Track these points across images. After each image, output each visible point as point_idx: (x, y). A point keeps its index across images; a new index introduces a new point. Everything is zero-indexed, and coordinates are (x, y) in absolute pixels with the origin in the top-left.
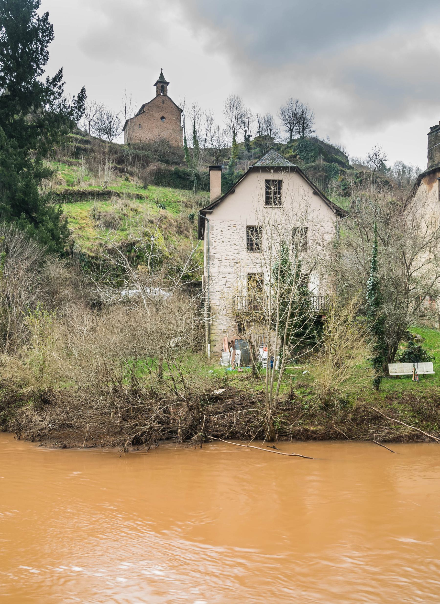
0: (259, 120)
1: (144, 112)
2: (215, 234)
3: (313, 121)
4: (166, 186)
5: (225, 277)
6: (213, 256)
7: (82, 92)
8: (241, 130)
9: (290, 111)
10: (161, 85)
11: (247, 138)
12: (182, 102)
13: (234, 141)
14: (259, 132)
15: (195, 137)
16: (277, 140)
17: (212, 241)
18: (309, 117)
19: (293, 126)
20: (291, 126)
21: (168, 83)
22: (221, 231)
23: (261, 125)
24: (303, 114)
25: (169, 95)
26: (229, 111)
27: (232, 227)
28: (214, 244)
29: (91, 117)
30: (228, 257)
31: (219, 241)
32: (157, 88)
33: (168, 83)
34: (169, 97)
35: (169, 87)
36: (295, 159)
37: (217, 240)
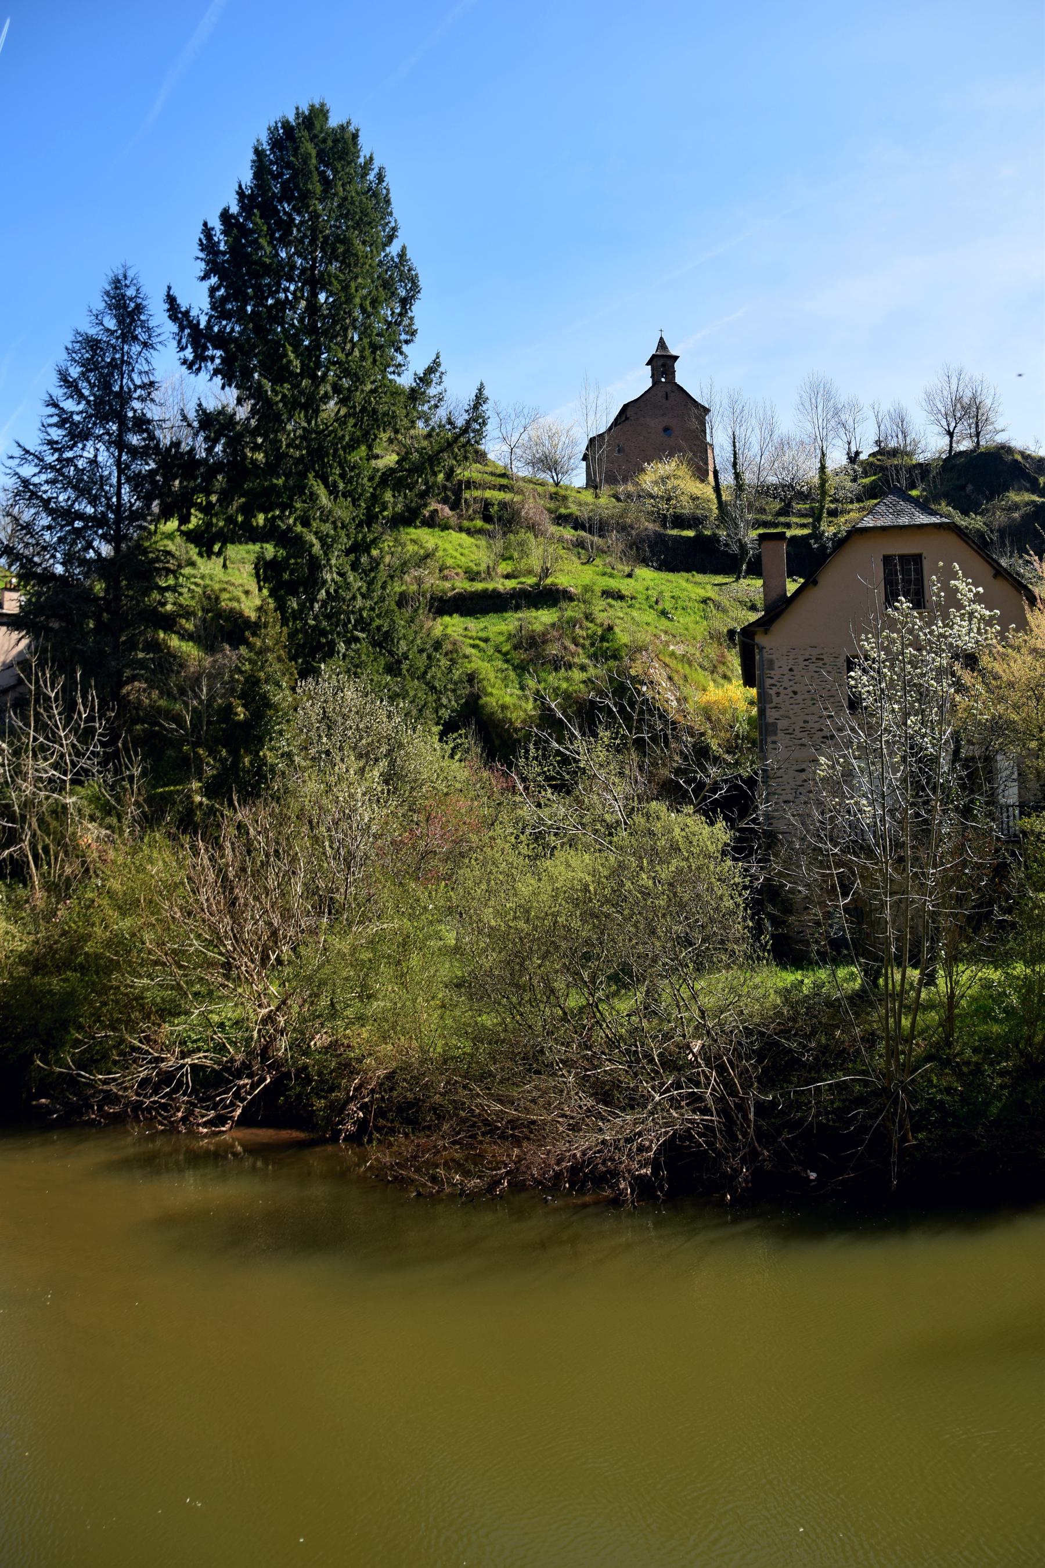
0: (877, 417)
1: (627, 419)
2: (776, 678)
3: (1000, 409)
4: (679, 571)
5: (803, 770)
6: (775, 725)
7: (480, 390)
8: (838, 442)
9: (946, 393)
10: (661, 362)
11: (853, 458)
12: (706, 391)
13: (823, 468)
14: (878, 442)
15: (735, 465)
16: (921, 456)
17: (771, 692)
18: (988, 402)
19: (953, 424)
20: (948, 425)
21: (676, 358)
22: (791, 670)
23: (882, 427)
24: (974, 398)
25: (679, 380)
26: (807, 405)
27: (814, 660)
28: (775, 699)
29: (514, 439)
30: (808, 726)
31: (786, 692)
32: (653, 370)
33: (676, 358)
34: (678, 386)
35: (677, 365)
36: (963, 494)
37: (781, 690)
